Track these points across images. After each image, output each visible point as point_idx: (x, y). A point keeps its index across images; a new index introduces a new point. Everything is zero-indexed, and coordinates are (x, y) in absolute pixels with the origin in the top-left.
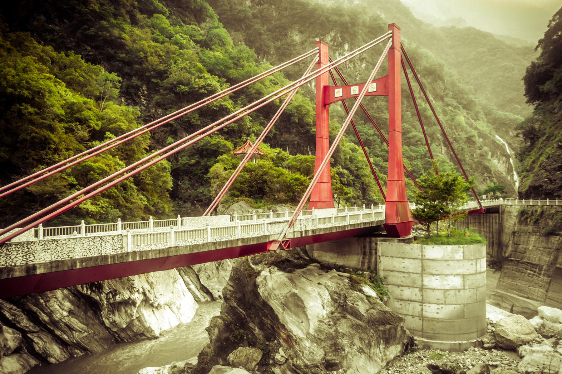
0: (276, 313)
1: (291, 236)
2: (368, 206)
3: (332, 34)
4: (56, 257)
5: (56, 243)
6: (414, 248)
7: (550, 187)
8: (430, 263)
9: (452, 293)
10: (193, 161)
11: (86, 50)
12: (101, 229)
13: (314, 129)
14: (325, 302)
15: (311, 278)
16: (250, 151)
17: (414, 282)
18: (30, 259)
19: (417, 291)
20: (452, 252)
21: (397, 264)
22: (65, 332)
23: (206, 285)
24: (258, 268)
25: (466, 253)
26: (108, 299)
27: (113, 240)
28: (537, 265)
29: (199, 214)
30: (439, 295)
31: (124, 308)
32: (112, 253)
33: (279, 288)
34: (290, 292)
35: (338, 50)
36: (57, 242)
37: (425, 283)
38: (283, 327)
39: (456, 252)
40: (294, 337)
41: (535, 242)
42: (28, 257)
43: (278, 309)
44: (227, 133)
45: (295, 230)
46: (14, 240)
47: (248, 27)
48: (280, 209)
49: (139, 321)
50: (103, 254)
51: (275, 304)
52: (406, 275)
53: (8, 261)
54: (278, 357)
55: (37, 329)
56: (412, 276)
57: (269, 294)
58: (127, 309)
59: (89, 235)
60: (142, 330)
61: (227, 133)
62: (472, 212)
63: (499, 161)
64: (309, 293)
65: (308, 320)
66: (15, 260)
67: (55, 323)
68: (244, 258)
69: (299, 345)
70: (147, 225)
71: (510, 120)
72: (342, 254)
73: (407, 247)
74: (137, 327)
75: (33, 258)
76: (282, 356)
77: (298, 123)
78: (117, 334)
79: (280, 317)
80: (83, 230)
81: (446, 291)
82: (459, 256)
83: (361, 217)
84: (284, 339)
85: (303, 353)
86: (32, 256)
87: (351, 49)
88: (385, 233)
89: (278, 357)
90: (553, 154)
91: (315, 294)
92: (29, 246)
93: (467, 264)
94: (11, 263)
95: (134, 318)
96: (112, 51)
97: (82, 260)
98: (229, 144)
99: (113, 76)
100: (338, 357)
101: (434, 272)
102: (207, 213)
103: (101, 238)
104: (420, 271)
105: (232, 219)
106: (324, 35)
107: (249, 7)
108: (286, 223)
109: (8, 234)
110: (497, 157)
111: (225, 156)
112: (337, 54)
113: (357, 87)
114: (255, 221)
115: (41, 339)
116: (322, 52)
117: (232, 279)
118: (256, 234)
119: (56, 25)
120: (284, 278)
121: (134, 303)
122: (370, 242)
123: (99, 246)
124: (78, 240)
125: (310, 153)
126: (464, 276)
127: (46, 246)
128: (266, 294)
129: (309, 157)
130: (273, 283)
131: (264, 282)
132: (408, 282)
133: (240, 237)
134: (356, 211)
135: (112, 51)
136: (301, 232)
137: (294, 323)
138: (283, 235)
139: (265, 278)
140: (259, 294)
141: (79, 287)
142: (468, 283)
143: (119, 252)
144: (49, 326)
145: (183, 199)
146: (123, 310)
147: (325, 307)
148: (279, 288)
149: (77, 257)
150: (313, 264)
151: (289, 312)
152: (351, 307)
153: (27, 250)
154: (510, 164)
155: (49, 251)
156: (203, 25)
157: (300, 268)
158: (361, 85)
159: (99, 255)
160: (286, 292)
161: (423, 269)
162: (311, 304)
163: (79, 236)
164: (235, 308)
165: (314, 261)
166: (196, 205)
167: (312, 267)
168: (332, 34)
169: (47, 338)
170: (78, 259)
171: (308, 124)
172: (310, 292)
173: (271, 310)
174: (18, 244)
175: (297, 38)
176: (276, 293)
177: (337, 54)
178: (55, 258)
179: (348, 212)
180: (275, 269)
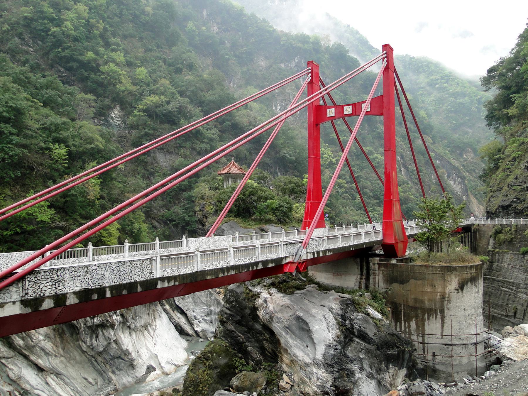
0: (278, 337)
3: (297, 60)
4: (86, 285)
5: (86, 269)
11: (60, 71)
14: (330, 325)
15: (314, 300)
18: (59, 288)
22: (39, 357)
23: (180, 306)
24: (257, 289)
27: (142, 264)
28: (513, 283)
31: (102, 332)
32: (141, 280)
33: (281, 311)
34: (293, 314)
36: (87, 267)
40: (299, 362)
41: (511, 260)
42: (57, 285)
43: (281, 333)
45: (309, 251)
46: (42, 268)
48: (271, 229)
49: (117, 344)
50: (133, 281)
51: (276, 327)
53: (37, 291)
54: (282, 383)
55: (12, 353)
57: (271, 318)
58: (104, 331)
60: (119, 353)
63: (455, 182)
64: (314, 316)
65: (314, 344)
66: (44, 289)
69: (305, 371)
71: (464, 143)
72: (338, 275)
74: (115, 350)
75: (62, 287)
76: (287, 383)
78: (94, 357)
79: (282, 341)
83: (363, 237)
84: (287, 364)
85: (310, 379)
86: (61, 284)
89: (282, 383)
90: (521, 175)
91: (320, 317)
92: (58, 274)
94: (39, 293)
95: (112, 341)
96: (86, 74)
97: (112, 288)
102: (211, 233)
107: (217, 33)
108: (300, 244)
110: (453, 178)
113: (351, 107)
115: (16, 365)
116: (313, 72)
119: (30, 46)
120: (286, 300)
121: (112, 326)
123: (128, 271)
124: (108, 265)
125: (279, 174)
127: (76, 273)
128: (267, 317)
130: (275, 306)
131: (265, 305)
133: (260, 260)
135: (86, 74)
136: (314, 253)
138: (298, 256)
139: (265, 301)
140: (259, 317)
143: (148, 278)
144: (24, 351)
145: (156, 219)
146: (101, 333)
147: (330, 330)
148: (281, 311)
149: (107, 285)
150: (312, 285)
151: (294, 337)
152: (358, 330)
153: (56, 278)
154: (465, 185)
155: (79, 278)
156: (174, 49)
159: (129, 281)
160: (289, 315)
162: (317, 327)
164: (233, 331)
166: (168, 225)
167: (310, 288)
168: (297, 60)
169: (20, 362)
170: (108, 287)
172: (315, 315)
173: (272, 333)
176: (279, 316)
178: (85, 286)
180: (273, 290)
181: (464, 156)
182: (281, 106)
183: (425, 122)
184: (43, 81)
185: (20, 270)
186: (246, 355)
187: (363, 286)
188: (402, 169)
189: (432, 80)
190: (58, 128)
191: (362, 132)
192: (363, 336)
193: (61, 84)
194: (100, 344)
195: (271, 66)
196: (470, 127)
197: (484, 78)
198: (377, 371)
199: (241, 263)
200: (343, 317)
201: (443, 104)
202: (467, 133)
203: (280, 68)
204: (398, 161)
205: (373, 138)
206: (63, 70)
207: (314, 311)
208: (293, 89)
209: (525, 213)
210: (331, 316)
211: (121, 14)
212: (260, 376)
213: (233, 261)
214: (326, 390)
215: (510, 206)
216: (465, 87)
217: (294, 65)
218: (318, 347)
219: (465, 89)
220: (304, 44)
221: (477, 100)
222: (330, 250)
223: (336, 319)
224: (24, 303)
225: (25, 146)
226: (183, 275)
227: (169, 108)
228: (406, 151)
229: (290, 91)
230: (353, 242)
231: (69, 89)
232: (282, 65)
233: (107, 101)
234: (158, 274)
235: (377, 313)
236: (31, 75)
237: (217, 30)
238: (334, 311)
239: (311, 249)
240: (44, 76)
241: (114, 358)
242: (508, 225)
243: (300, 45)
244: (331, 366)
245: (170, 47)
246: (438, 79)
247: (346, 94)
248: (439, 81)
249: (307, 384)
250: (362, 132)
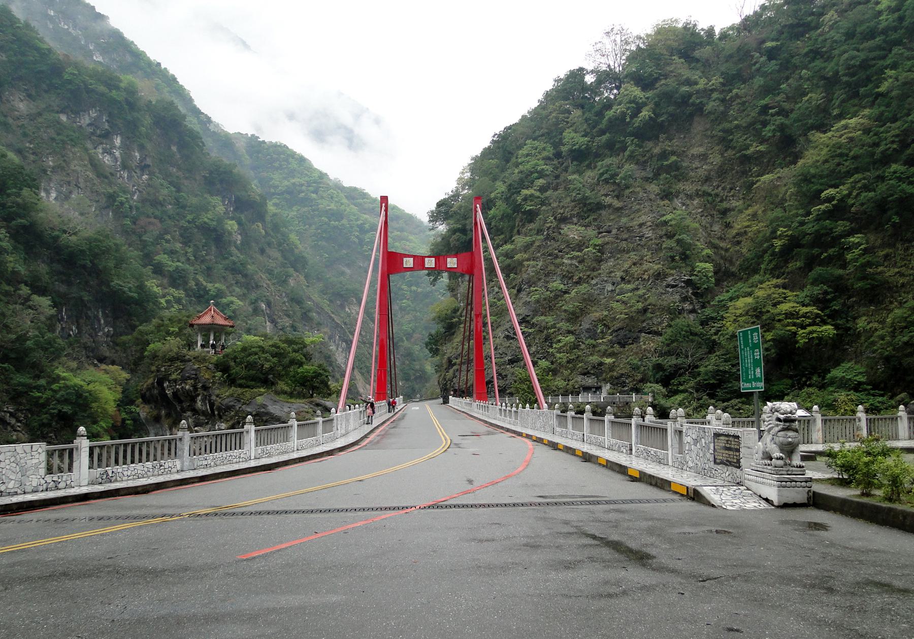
35: (102, 143)
70: (171, 449)
71: (347, 290)
100: (637, 283)
181: (347, 310)
182: (59, 192)
183: (296, 251)
189: (294, 184)
191: (207, 258)
195: (40, 114)
196: (348, 265)
197: (432, 212)
201: (310, 225)
202: (343, 273)
203: (59, 122)
204: (263, 311)
208: (85, 166)
209: (508, 392)
216: (342, 204)
217: (88, 121)
219: (343, 207)
220: (110, 90)
221: (358, 226)
228: (275, 295)
229: (78, 168)
232: (64, 118)
243: (102, 88)
246: (302, 185)
247: (179, 190)
248: (304, 188)
250: (207, 258)
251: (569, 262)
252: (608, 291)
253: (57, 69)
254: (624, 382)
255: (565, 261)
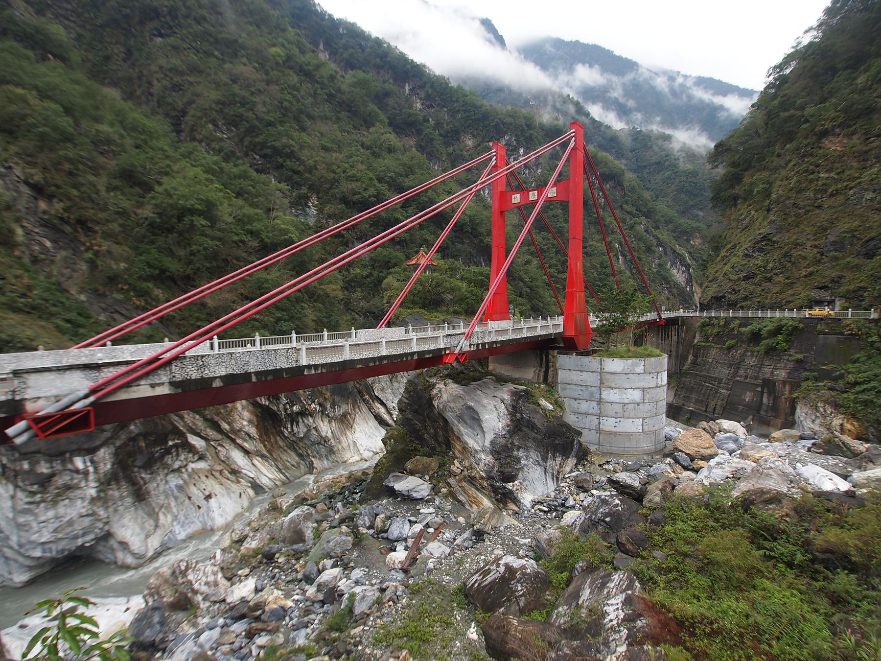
1: (468, 349)
2: (545, 318)
3: (507, 138)
6: (591, 362)
7: (733, 297)
8: (608, 376)
9: (631, 406)
10: (365, 273)
12: (276, 342)
13: (487, 239)
15: (488, 391)
16: (423, 261)
17: (592, 395)
19: (595, 403)
20: (633, 365)
21: (575, 377)
22: (245, 440)
25: (647, 366)
26: (286, 410)
28: (716, 378)
29: (374, 326)
30: (618, 408)
37: (603, 396)
38: (459, 439)
39: (637, 365)
44: (399, 243)
46: (187, 354)
47: (419, 132)
49: (316, 431)
51: (449, 416)
52: (583, 388)
55: (220, 437)
56: (590, 389)
59: (263, 348)
61: (399, 243)
62: (651, 324)
65: (483, 432)
67: (237, 432)
68: (418, 371)
70: (321, 338)
73: (586, 360)
77: (471, 233)
80: (258, 343)
81: (625, 404)
82: (640, 369)
83: (538, 329)
87: (526, 153)
88: (562, 345)
89: (453, 468)
91: (491, 407)
93: (648, 377)
96: (281, 160)
97: (257, 373)
98: (401, 255)
99: (283, 186)
101: (613, 385)
103: (275, 350)
104: (598, 385)
105: (407, 331)
106: (498, 140)
107: (420, 110)
109: (184, 346)
111: (396, 269)
112: (512, 160)
114: (430, 333)
117: (407, 391)
118: (432, 347)
122: (547, 356)
126: (643, 389)
128: (441, 406)
129: (485, 269)
132: (585, 395)
134: (532, 323)
135: (281, 160)
136: (478, 345)
137: (469, 435)
139: (440, 391)
141: (258, 399)
142: (647, 396)
148: (454, 401)
154: (689, 274)
156: (372, 130)
157: (475, 381)
158: (540, 188)
161: (602, 383)
163: (253, 349)
165: (489, 373)
168: (507, 138)
169: (227, 445)
171: (481, 234)
173: (446, 421)
174: (196, 358)
175: (470, 143)
177: (512, 160)
178: (230, 371)
179: (523, 324)
184: (235, 170)
185: (168, 355)
186: (421, 440)
187: (541, 379)
188: (620, 257)
190: (251, 220)
192: (532, 426)
193: (255, 174)
194: (301, 430)
195: (479, 145)
196: (701, 209)
198: (543, 459)
199: (394, 353)
200: (514, 407)
205: (589, 223)
206: (258, 157)
207: (485, 401)
210: (503, 406)
211: (315, 93)
212: (433, 463)
213: (385, 352)
214: (492, 474)
215: (724, 297)
218: (486, 435)
222: (496, 342)
223: (507, 410)
224: (172, 384)
225: (220, 239)
226: (332, 365)
227: (366, 194)
230: (539, 332)
231: (263, 177)
233: (304, 190)
234: (304, 362)
235: (548, 404)
236: (224, 164)
237: (421, 107)
238: (505, 402)
239: (474, 341)
240: (236, 166)
241: (313, 444)
242: (717, 318)
244: (498, 453)
245: (368, 128)
249: (476, 469)
251: (826, 175)
252: (867, 200)
253: (486, 116)
254: (861, 296)
255: (822, 175)
